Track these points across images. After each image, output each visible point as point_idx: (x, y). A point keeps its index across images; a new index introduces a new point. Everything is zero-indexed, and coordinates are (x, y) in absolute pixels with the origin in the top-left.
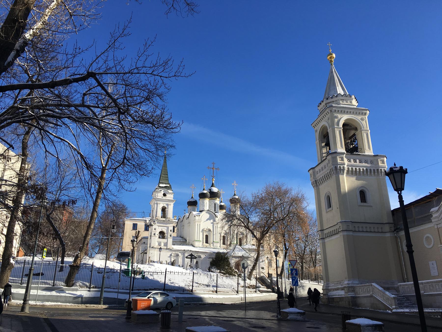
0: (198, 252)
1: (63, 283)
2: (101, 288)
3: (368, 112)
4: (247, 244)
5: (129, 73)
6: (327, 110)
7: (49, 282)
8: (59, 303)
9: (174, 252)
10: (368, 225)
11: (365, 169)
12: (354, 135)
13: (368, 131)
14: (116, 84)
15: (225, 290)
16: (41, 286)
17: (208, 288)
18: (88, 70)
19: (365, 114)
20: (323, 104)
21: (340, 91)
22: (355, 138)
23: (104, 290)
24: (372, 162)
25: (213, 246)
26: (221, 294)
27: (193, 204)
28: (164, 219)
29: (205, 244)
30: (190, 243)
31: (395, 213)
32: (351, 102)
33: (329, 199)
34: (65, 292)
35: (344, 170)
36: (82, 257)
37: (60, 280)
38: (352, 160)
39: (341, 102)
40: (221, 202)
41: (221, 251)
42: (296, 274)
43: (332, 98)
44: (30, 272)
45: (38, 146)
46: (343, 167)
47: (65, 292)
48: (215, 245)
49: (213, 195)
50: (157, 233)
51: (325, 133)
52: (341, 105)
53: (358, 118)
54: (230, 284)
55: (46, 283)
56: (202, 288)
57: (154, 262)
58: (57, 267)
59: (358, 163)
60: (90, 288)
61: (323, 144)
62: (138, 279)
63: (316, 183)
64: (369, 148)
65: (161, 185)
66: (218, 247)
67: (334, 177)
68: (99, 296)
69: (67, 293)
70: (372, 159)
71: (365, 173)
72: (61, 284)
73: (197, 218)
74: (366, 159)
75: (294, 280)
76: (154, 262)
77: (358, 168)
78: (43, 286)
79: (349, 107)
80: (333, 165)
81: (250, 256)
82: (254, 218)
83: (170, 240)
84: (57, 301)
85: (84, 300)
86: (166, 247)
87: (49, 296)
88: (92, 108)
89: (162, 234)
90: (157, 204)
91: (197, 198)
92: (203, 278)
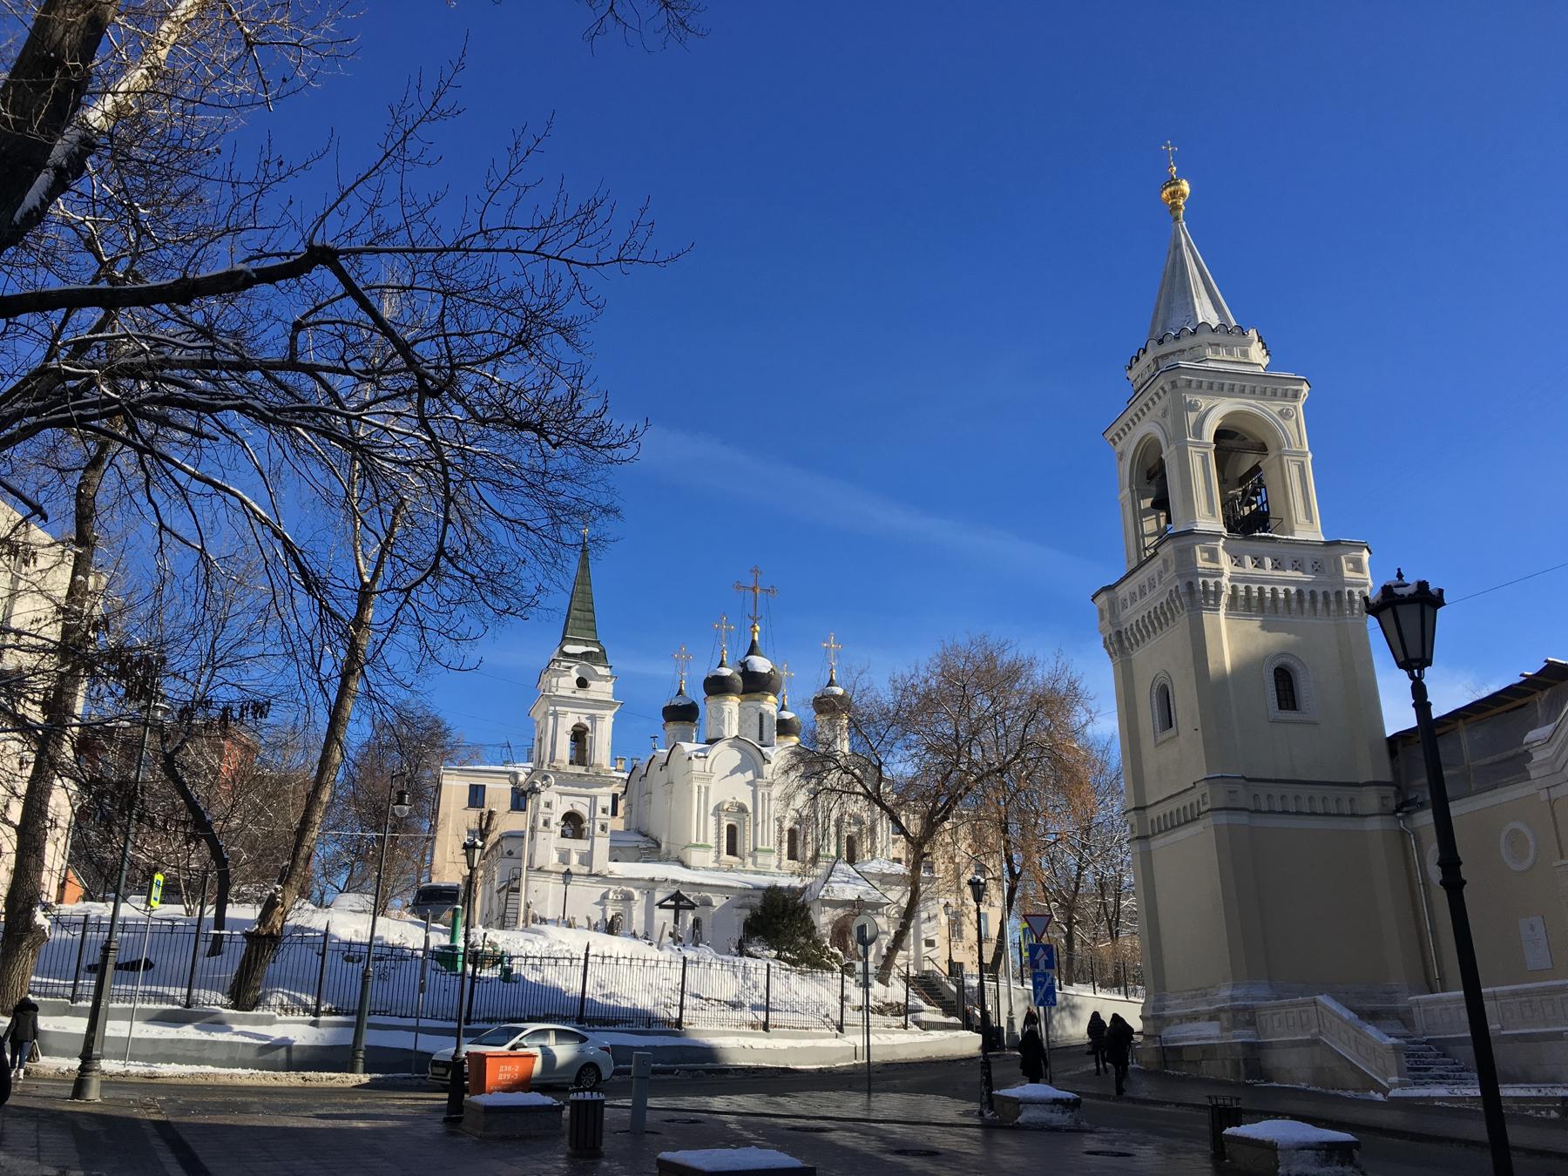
0: (701, 885)
1: (220, 998)
2: (358, 1014)
3: (1305, 388)
4: (873, 857)
5: (457, 249)
6: (1161, 382)
7: (171, 991)
8: (209, 1069)
9: (614, 887)
10: (1306, 791)
11: (1293, 590)
12: (1256, 469)
13: (1304, 454)
14: (411, 287)
15: (788, 1021)
16: (145, 1006)
17: (737, 1015)
18: (311, 241)
19: (1296, 395)
20: (1146, 360)
21: (1205, 312)
22: (1260, 480)
23: (368, 1019)
24: (1317, 568)
25: (754, 863)
26: (783, 1036)
27: (682, 714)
28: (580, 770)
29: (724, 856)
30: (674, 855)
31: (1399, 747)
32: (1245, 354)
33: (1164, 697)
34: (230, 1030)
35: (1217, 594)
36: (288, 904)
37: (211, 986)
38: (1248, 559)
39: (1209, 353)
40: (783, 708)
41: (783, 882)
42: (1050, 965)
43: (1177, 338)
44: (105, 958)
45: (134, 510)
46: (1217, 584)
47: (230, 1030)
48: (760, 860)
49: (755, 685)
50: (556, 818)
51: (1151, 462)
52: (1211, 364)
53: (1268, 409)
54: (815, 997)
55: (161, 998)
56: (713, 1012)
57: (544, 921)
58: (202, 938)
59: (1268, 569)
60: (317, 1013)
61: (1146, 503)
62: (488, 981)
63: (1121, 642)
64: (1309, 515)
65: (569, 649)
66: (773, 869)
67: (1183, 619)
68: (350, 1042)
69: (237, 1033)
70: (1320, 554)
71: (1294, 605)
72: (213, 999)
73: (697, 765)
74: (1297, 555)
75: (1041, 984)
76: (544, 921)
77: (1268, 588)
78: (152, 1006)
79: (1238, 371)
80: (1180, 576)
81: (885, 900)
82: (901, 766)
83: (602, 845)
84: (199, 1061)
85: (295, 1055)
86: (585, 870)
87: (172, 1041)
88: (324, 375)
89: (573, 824)
90: (556, 715)
91: (697, 694)
92: (719, 977)
